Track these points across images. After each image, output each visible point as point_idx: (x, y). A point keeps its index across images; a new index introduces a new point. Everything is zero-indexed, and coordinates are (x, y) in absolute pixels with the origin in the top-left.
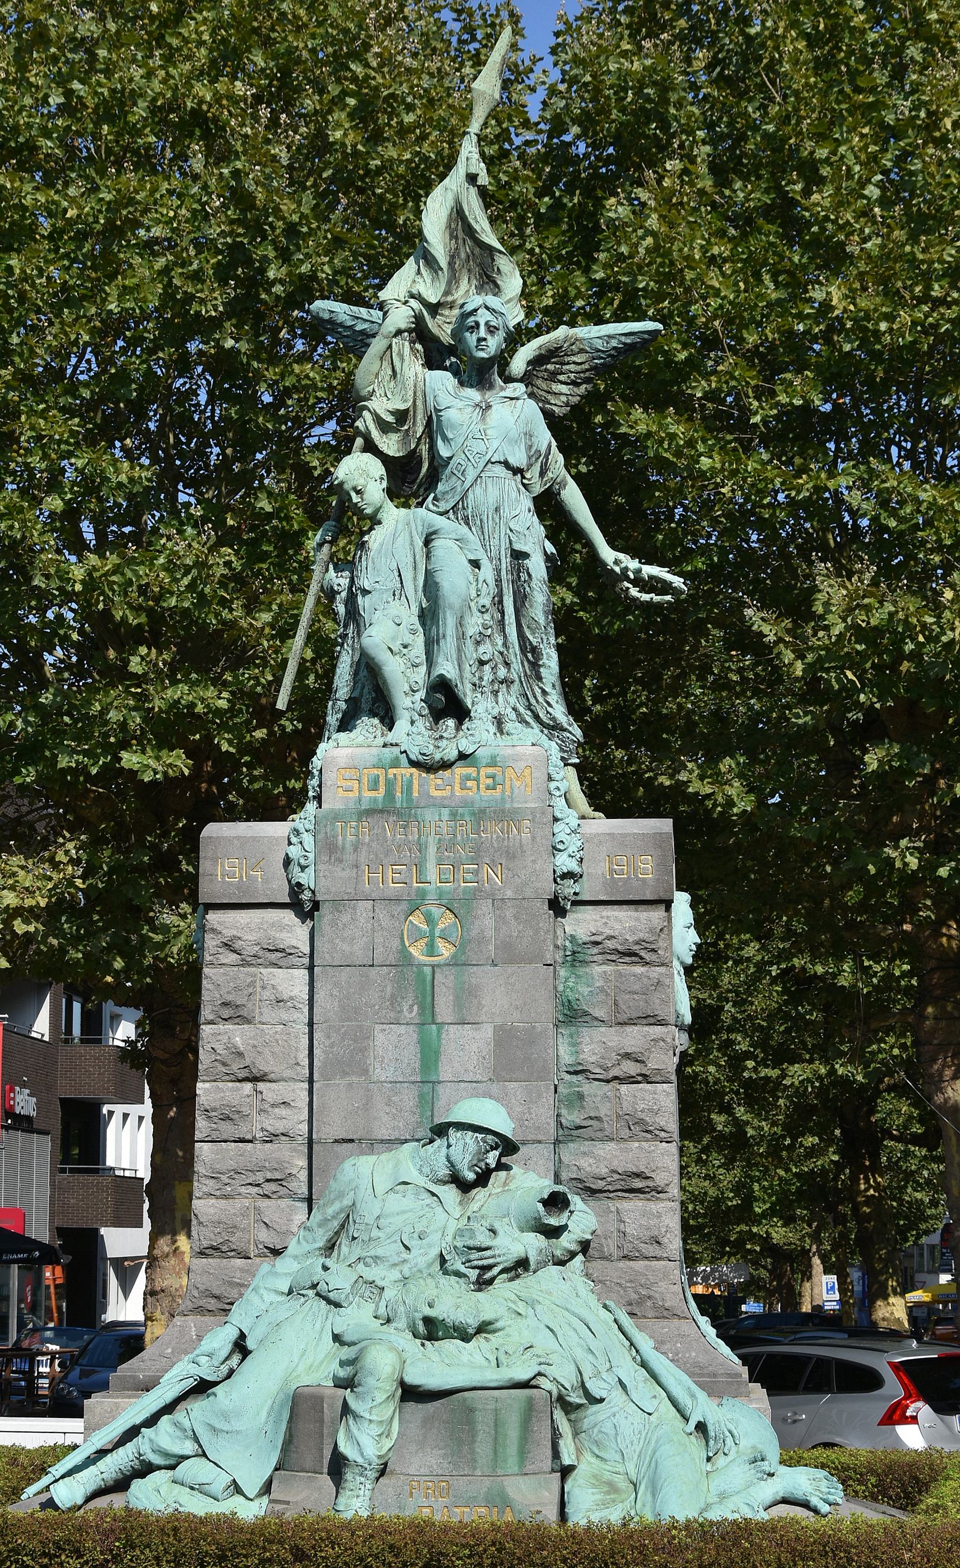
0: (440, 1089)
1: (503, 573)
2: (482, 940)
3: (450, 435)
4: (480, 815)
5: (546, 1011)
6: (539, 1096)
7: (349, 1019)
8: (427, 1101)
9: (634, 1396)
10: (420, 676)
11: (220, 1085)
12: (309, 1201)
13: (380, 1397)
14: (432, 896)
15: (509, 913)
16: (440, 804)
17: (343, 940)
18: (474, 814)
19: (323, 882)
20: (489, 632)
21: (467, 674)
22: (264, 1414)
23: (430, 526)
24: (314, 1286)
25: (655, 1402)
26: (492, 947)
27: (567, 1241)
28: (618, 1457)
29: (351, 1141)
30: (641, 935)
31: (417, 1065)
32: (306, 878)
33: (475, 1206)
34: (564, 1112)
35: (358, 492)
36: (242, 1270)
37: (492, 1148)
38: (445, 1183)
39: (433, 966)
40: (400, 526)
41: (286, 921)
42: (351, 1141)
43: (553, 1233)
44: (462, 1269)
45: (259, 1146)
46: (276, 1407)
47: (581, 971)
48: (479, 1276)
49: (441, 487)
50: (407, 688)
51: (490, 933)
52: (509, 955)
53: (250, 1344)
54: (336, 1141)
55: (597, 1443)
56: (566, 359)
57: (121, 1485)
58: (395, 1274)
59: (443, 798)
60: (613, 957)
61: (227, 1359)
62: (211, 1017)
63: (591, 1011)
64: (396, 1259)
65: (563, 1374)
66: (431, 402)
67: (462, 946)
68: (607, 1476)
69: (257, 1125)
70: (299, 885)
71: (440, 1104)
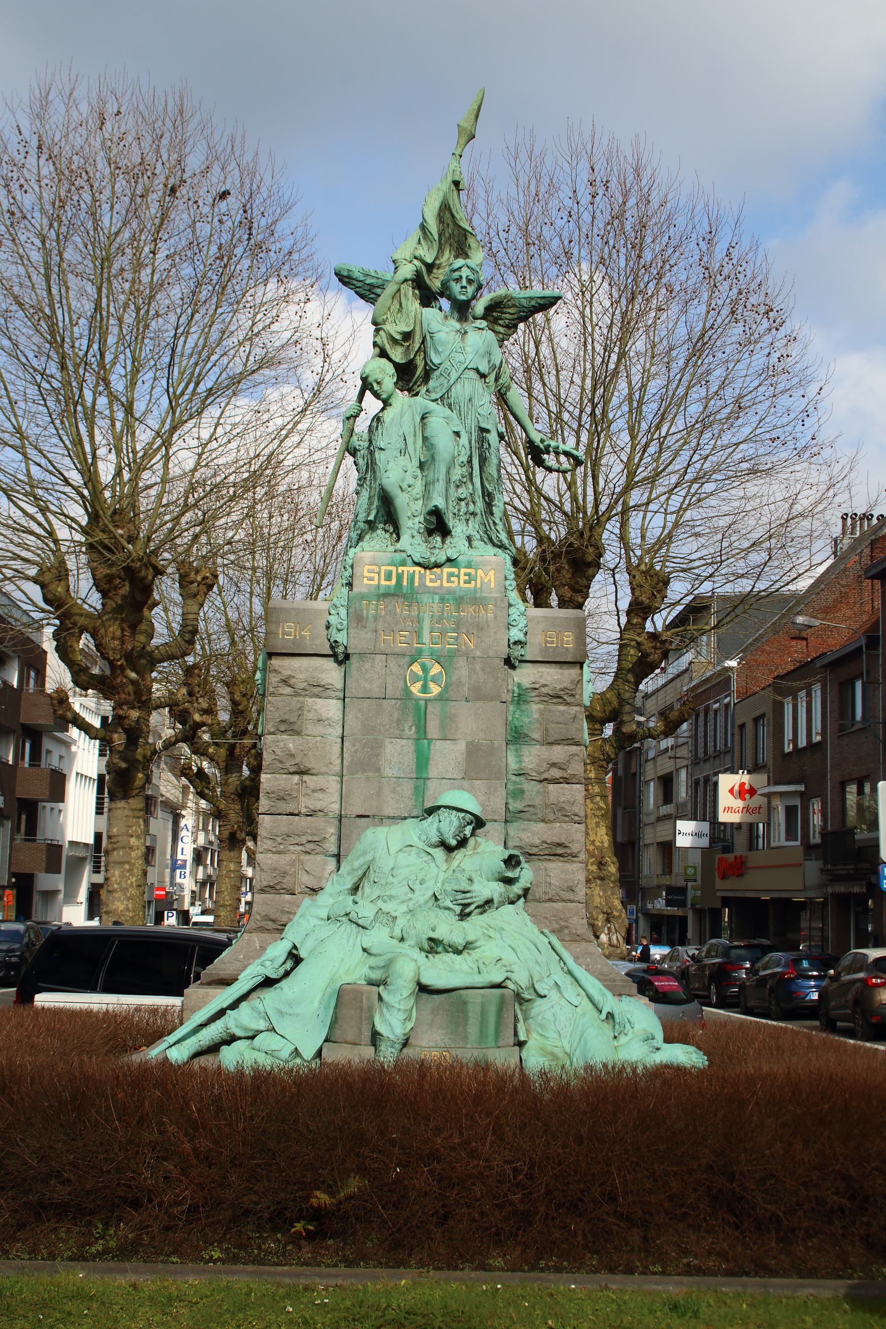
0: (429, 783)
2: (459, 684)
3: (440, 349)
4: (460, 600)
5: (500, 734)
6: (496, 790)
7: (368, 734)
8: (420, 791)
9: (565, 994)
11: (277, 776)
12: (338, 857)
13: (406, 993)
14: (426, 653)
15: (478, 667)
16: (433, 592)
17: (366, 680)
18: (456, 599)
19: (352, 641)
21: (451, 507)
22: (316, 1004)
23: (426, 408)
24: (347, 914)
25: (579, 998)
26: (466, 689)
27: (517, 889)
28: (556, 1036)
29: (368, 816)
30: (565, 685)
31: (414, 767)
32: (342, 638)
33: (455, 863)
34: (510, 801)
35: (378, 383)
36: (290, 903)
37: (469, 824)
38: (436, 847)
39: (426, 701)
40: (406, 407)
41: (325, 666)
42: (368, 816)
43: (509, 881)
44: (451, 905)
45: (303, 818)
46: (326, 998)
47: (524, 707)
48: (462, 910)
49: (431, 383)
50: (409, 514)
51: (465, 679)
52: (478, 695)
53: (303, 954)
54: (358, 816)
55: (541, 1026)
57: (213, 1049)
58: (404, 908)
59: (435, 588)
61: (284, 963)
62: (272, 730)
64: (405, 898)
65: (521, 979)
66: (425, 325)
67: (446, 689)
68: (549, 1048)
69: (305, 803)
70: (336, 642)
71: (429, 793)
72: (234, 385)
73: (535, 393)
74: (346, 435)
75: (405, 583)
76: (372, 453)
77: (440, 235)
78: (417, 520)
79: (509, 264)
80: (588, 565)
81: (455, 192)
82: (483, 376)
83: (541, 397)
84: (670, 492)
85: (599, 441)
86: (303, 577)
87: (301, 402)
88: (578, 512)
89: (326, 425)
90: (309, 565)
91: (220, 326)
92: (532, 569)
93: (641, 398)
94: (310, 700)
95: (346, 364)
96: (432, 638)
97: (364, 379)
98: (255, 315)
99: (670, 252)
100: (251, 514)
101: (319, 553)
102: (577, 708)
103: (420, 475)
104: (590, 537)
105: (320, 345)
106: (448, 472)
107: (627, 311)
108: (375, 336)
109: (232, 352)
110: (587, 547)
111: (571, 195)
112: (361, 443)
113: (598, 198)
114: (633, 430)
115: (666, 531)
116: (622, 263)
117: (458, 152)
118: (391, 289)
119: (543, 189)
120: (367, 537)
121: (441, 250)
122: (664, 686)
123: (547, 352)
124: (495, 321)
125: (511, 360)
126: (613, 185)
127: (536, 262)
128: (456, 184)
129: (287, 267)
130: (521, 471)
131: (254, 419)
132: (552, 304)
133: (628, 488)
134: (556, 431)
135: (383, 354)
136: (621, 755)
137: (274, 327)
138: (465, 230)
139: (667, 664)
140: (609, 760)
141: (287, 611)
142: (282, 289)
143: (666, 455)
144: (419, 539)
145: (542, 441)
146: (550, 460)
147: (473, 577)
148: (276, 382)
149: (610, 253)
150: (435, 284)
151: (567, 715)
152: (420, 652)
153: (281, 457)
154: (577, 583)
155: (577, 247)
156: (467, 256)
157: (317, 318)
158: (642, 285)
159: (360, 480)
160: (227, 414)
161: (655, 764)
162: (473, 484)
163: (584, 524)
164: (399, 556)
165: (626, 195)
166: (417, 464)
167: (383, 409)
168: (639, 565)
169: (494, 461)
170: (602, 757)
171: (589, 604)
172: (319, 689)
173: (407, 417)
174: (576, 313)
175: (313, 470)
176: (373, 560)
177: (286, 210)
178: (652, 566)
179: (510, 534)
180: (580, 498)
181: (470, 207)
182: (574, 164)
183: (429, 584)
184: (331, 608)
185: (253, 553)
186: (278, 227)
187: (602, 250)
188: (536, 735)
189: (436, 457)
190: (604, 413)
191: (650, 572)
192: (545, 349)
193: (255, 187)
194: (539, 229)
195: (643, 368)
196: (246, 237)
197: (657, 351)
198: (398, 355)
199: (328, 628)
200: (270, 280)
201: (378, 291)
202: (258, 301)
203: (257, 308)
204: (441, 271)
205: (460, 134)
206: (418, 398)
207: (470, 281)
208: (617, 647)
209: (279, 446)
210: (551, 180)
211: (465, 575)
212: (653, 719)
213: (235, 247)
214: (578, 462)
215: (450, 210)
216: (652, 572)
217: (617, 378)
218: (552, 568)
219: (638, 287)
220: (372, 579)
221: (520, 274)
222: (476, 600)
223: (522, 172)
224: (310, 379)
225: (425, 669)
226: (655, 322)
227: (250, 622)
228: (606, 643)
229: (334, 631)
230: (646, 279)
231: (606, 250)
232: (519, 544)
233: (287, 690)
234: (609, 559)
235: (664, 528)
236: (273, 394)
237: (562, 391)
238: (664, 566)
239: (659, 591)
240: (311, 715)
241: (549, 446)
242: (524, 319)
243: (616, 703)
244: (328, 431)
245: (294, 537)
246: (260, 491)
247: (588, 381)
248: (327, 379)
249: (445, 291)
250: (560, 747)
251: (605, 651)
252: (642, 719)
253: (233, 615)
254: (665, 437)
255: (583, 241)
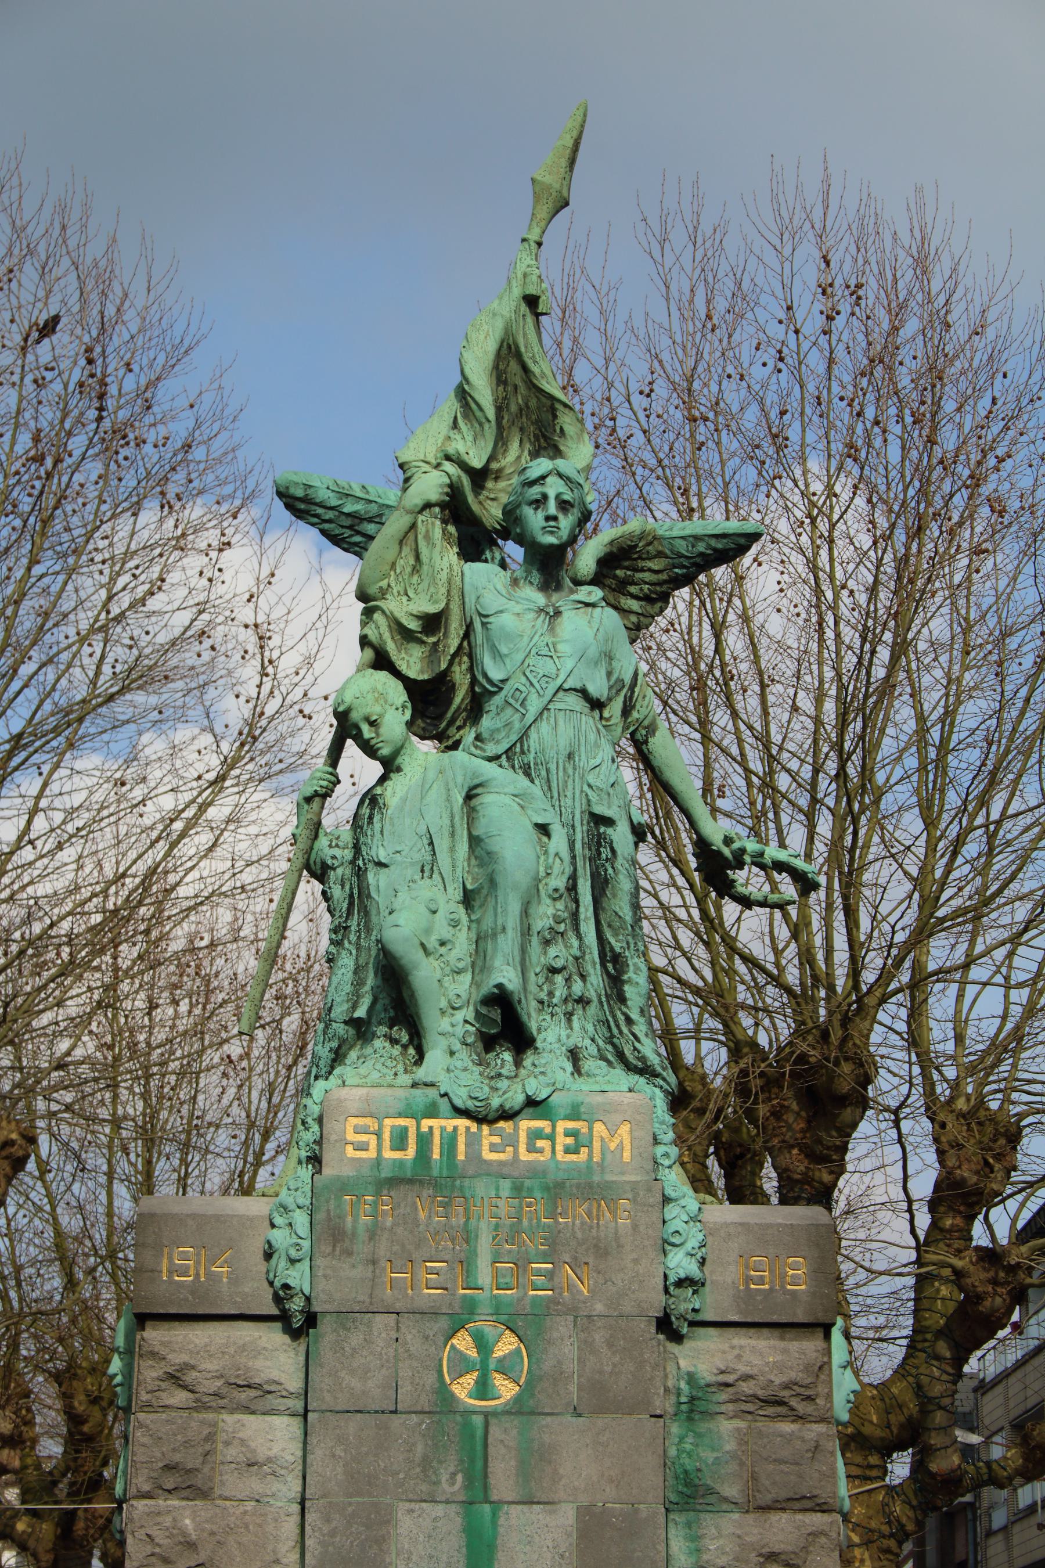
1: (578, 846)
3: (504, 650)
4: (558, 1190)
5: (650, 1487)
10: (462, 985)
14: (485, 1309)
15: (599, 1337)
16: (497, 1172)
18: (546, 1188)
19: (322, 1284)
20: (562, 927)
21: (532, 988)
23: (475, 775)
26: (573, 1388)
30: (793, 1375)
32: (298, 1277)
35: (373, 724)
40: (431, 775)
47: (703, 1426)
49: (486, 722)
50: (443, 1004)
51: (571, 1366)
52: (599, 1401)
56: (641, 564)
59: (501, 1163)
60: (750, 1407)
62: (146, 1487)
63: (718, 1487)
67: (529, 1388)
70: (286, 1287)
72: (67, 727)
73: (716, 733)
74: (304, 834)
75: (436, 1156)
76: (360, 873)
77: (499, 410)
78: (460, 1016)
79: (653, 462)
80: (842, 1101)
81: (530, 319)
82: (596, 705)
83: (729, 741)
84: (1015, 940)
85: (855, 833)
86: (222, 1138)
87: (215, 761)
88: (815, 986)
89: (268, 809)
90: (235, 1110)
91: (36, 603)
92: (720, 1111)
93: (945, 740)
94: (229, 1420)
95: (310, 678)
96: (496, 1274)
97: (342, 716)
98: (113, 580)
99: (996, 429)
100: (108, 1001)
101: (258, 1083)
102: (821, 1428)
103: (465, 919)
104: (844, 1040)
105: (254, 639)
106: (525, 913)
107: (907, 556)
108: (364, 624)
109: (65, 657)
110: (837, 1063)
111: (782, 315)
112: (337, 852)
113: (840, 321)
114: (930, 807)
115: (1009, 1026)
116: (894, 453)
117: (534, 236)
118: (395, 524)
119: (721, 305)
120: (353, 1055)
121: (501, 441)
122: (1020, 1364)
123: (740, 645)
124: (621, 587)
125: (663, 664)
126: (870, 293)
127: (709, 457)
128: (531, 301)
129: (180, 476)
130: (691, 900)
131: (113, 797)
132: (743, 550)
133: (924, 931)
134: (764, 813)
135: (382, 662)
136: (931, 1522)
137: (152, 604)
138: (552, 398)
139: (1025, 1315)
140: (901, 1535)
141: (179, 1220)
142: (170, 523)
143: (1002, 862)
144: (464, 1058)
145: (728, 841)
146: (749, 880)
147: (583, 1139)
148: (161, 719)
149: (868, 434)
150: (492, 513)
151: (798, 1444)
152: (470, 1308)
153: (172, 878)
154: (819, 1141)
155: (797, 425)
156: (557, 452)
157: (245, 583)
158: (938, 502)
159: (335, 931)
160: (54, 787)
161: (1008, 1540)
162: (579, 937)
163: (830, 1013)
164: (421, 1096)
165: (898, 312)
166: (458, 895)
167: (383, 779)
168: (951, 1100)
169: (625, 885)
170: (886, 1529)
171: (847, 1188)
172: (251, 1394)
173: (435, 794)
174: (799, 562)
175: (241, 905)
176: (366, 1105)
177: (179, 354)
178: (982, 1102)
179: (668, 1036)
180: (820, 956)
181: (567, 344)
182: (787, 251)
183: (488, 1156)
184: (279, 1208)
185: (114, 1086)
186: (160, 394)
187: (852, 429)
188: (731, 1490)
189: (499, 879)
190: (866, 772)
191: (975, 1115)
192: (734, 641)
193: (111, 311)
194: (714, 388)
195: (948, 675)
196: (92, 414)
197: (975, 640)
198: (413, 663)
199: (268, 1256)
200: (146, 504)
201: (370, 528)
202: (120, 549)
203: (118, 564)
204: (502, 484)
205: (537, 197)
206: (459, 754)
207: (564, 505)
208: (911, 1281)
209: (168, 854)
210: (739, 284)
211: (567, 1134)
212: (997, 1439)
213: (69, 434)
214: (806, 884)
215: (518, 356)
216: (982, 1113)
217: (892, 699)
218: (763, 1110)
219: (929, 504)
220: (363, 1147)
221: (678, 481)
222: (590, 1188)
223: (676, 269)
224: (233, 713)
225: (482, 1345)
226: (968, 579)
227: (109, 1237)
228: (886, 1273)
229: (283, 1263)
230: (947, 487)
231: (859, 429)
232: (689, 1058)
233: (180, 1397)
234: (885, 1087)
235: (1004, 1018)
236: (153, 745)
237: (773, 728)
238: (1007, 1100)
239: (999, 1157)
240: (232, 1453)
241: (743, 851)
242: (687, 580)
243: (913, 1407)
244: (270, 819)
245: (201, 1053)
246: (128, 953)
247: (830, 706)
248: (269, 711)
249: (511, 527)
250: (785, 1516)
251: (885, 1289)
252: (975, 1439)
253: (71, 1223)
254: (999, 823)
255: (808, 411)
